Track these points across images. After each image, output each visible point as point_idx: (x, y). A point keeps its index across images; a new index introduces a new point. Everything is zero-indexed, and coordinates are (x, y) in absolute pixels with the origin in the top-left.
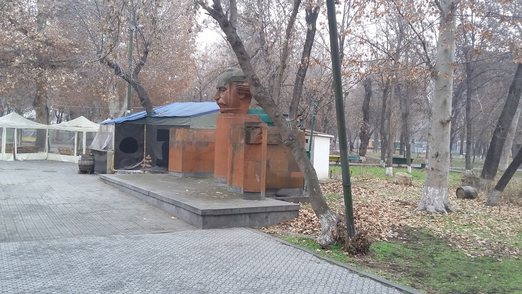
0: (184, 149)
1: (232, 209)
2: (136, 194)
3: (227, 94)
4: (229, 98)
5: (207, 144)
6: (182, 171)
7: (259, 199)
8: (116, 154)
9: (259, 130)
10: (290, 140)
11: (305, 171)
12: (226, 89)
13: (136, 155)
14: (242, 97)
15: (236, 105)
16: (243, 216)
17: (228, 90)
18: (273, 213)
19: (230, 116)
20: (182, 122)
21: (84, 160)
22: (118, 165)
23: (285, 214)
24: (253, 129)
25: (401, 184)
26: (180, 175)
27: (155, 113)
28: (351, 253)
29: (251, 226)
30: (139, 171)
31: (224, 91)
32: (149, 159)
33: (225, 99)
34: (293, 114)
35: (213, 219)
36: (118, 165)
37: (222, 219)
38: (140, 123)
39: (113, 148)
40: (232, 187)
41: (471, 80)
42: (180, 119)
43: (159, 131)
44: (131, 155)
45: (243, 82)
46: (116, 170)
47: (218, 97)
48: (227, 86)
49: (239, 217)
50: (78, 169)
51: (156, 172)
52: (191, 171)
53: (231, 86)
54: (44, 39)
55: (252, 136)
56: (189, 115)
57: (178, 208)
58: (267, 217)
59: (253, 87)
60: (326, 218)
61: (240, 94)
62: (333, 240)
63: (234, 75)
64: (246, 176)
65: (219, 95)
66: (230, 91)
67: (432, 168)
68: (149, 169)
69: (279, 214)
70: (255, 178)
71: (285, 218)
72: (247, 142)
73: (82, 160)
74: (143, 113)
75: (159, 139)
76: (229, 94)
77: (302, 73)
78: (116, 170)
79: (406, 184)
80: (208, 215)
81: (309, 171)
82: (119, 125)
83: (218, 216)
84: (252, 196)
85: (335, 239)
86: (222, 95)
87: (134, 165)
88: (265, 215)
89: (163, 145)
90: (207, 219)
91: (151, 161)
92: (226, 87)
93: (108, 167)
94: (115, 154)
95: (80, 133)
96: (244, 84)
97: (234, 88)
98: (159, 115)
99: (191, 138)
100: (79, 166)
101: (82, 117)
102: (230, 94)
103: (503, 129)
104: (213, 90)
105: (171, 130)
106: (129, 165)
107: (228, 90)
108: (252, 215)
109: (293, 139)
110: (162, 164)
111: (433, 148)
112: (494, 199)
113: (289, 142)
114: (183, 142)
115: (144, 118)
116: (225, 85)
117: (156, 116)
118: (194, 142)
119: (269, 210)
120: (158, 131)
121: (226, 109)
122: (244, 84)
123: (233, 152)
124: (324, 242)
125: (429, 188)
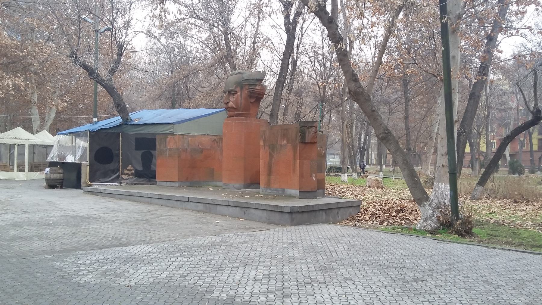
0: (179, 157)
1: (313, 206)
2: (161, 201)
3: (238, 97)
4: (240, 102)
5: (202, 151)
6: (178, 179)
8: (91, 165)
9: (314, 129)
10: (385, 133)
11: (403, 163)
12: (236, 92)
13: (112, 166)
14: (253, 100)
15: (247, 109)
17: (239, 94)
19: (241, 120)
20: (165, 129)
21: (53, 173)
22: (93, 178)
24: (308, 128)
25: (373, 187)
26: (177, 185)
28: (461, 235)
29: (327, 222)
30: (116, 184)
31: (234, 94)
32: (130, 170)
33: (236, 102)
34: (274, 120)
35: (298, 216)
37: (306, 216)
39: (88, 159)
40: (270, 189)
41: (408, 90)
42: (151, 127)
43: (136, 139)
44: (107, 166)
45: (256, 85)
46: (91, 184)
47: (228, 101)
48: (238, 89)
49: (318, 212)
50: (44, 184)
52: (187, 179)
53: (242, 89)
54: (252, 20)
55: (307, 135)
56: (172, 121)
57: (245, 210)
58: (338, 213)
59: (353, 82)
60: (430, 205)
61: (251, 97)
62: (439, 225)
63: (246, 78)
64: (302, 176)
65: (228, 99)
66: (241, 95)
67: (443, 166)
69: (346, 209)
70: (311, 177)
71: (350, 213)
72: (303, 142)
73: (51, 173)
74: (117, 120)
76: (240, 98)
77: (283, 80)
78: (91, 184)
79: (378, 187)
81: (407, 162)
82: (93, 134)
83: (303, 212)
84: (308, 194)
85: (441, 224)
86: (232, 99)
87: (110, 177)
88: (336, 211)
89: (143, 154)
90: (294, 216)
91: (133, 171)
94: (90, 165)
95: (22, 146)
96: (257, 87)
97: (246, 92)
98: (137, 122)
99: (185, 145)
100: (46, 180)
101: (19, 129)
102: (241, 97)
103: (465, 132)
105: (158, 138)
106: (105, 177)
107: (239, 94)
108: (327, 211)
109: (388, 133)
110: (147, 175)
111: (442, 147)
112: (477, 194)
113: (384, 135)
115: (120, 126)
116: (235, 88)
117: (134, 123)
118: (189, 150)
120: (136, 139)
121: (236, 113)
122: (257, 87)
123: (270, 154)
124: (429, 228)
125: (440, 184)
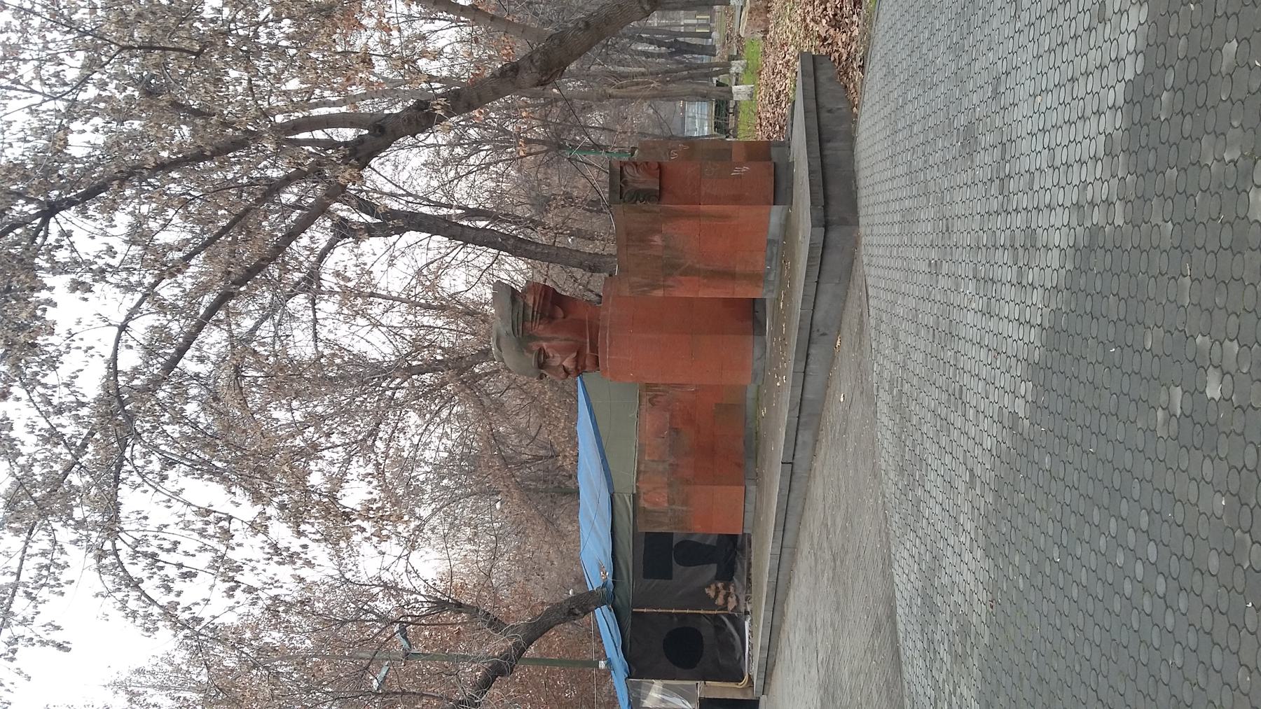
0: (687, 482)
1: (810, 173)
7: (790, 166)
12: (541, 350)
13: (707, 632)
16: (826, 152)
17: (544, 345)
18: (821, 100)
22: (735, 674)
23: (822, 78)
24: (625, 183)
25: (767, 21)
27: (604, 586)
30: (747, 624)
31: (546, 356)
32: (717, 591)
33: (564, 351)
35: (834, 207)
36: (735, 674)
37: (834, 190)
38: (628, 621)
42: (617, 518)
45: (525, 305)
46: (746, 677)
48: (535, 346)
49: (827, 161)
51: (749, 580)
53: (533, 338)
55: (642, 187)
56: (608, 495)
57: (815, 335)
58: (830, 111)
61: (552, 317)
63: (509, 328)
64: (737, 199)
66: (547, 340)
68: (742, 598)
71: (831, 79)
72: (658, 196)
74: (603, 617)
75: (667, 575)
76: (554, 343)
77: (511, 242)
78: (746, 677)
80: (825, 216)
82: (634, 670)
83: (826, 197)
86: (556, 360)
88: (824, 115)
90: (833, 218)
92: (535, 348)
93: (739, 696)
94: (705, 680)
97: (540, 329)
99: (661, 468)
102: (553, 339)
104: (545, 390)
105: (644, 529)
106: (733, 648)
107: (544, 345)
108: (824, 137)
110: (728, 555)
114: (670, 485)
116: (531, 352)
117: (610, 579)
118: (672, 460)
119: (814, 106)
121: (588, 351)
122: (530, 303)
